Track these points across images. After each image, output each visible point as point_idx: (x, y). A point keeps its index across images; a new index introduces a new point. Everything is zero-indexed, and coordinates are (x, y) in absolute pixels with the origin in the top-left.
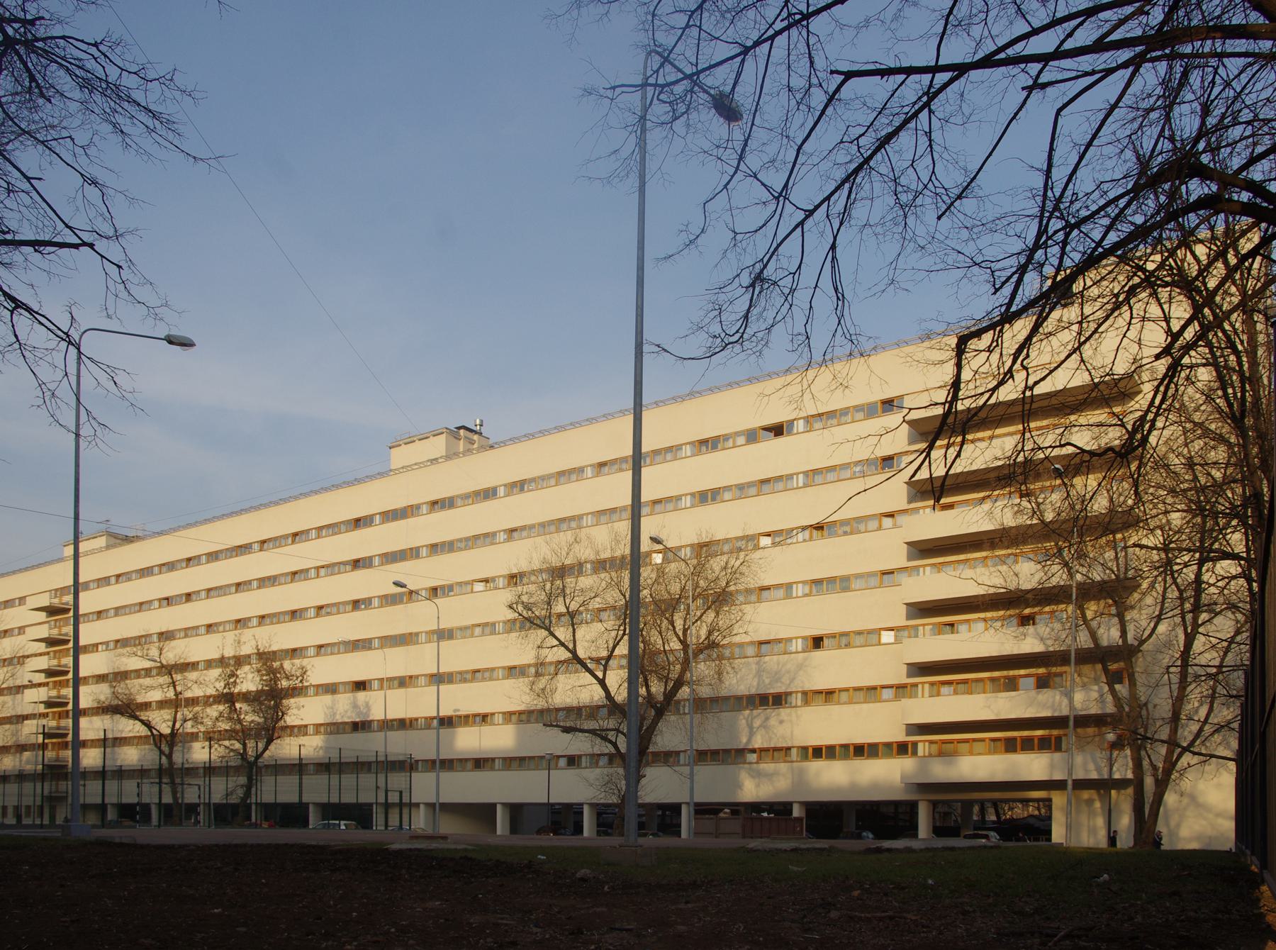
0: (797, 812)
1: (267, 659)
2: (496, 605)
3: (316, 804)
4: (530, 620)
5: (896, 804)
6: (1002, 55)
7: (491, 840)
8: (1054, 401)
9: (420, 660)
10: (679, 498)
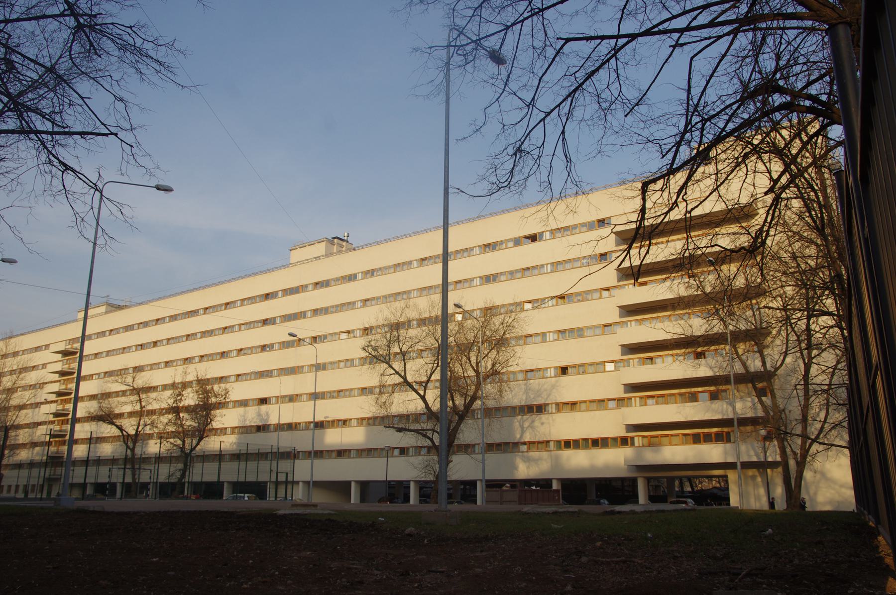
0: (555, 486)
1: (203, 384)
2: (354, 348)
3: (229, 482)
4: (376, 357)
5: (622, 480)
6: (656, 29)
7: (346, 507)
8: (704, 220)
9: (303, 384)
10: (472, 280)
